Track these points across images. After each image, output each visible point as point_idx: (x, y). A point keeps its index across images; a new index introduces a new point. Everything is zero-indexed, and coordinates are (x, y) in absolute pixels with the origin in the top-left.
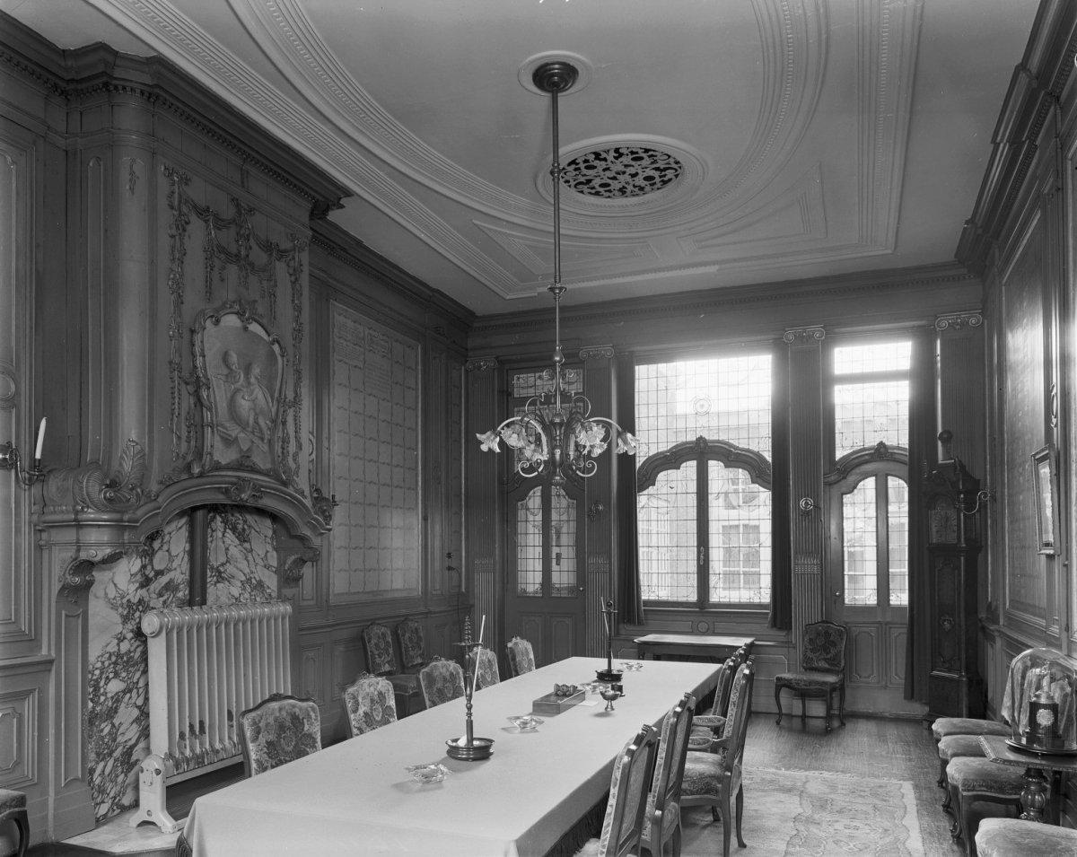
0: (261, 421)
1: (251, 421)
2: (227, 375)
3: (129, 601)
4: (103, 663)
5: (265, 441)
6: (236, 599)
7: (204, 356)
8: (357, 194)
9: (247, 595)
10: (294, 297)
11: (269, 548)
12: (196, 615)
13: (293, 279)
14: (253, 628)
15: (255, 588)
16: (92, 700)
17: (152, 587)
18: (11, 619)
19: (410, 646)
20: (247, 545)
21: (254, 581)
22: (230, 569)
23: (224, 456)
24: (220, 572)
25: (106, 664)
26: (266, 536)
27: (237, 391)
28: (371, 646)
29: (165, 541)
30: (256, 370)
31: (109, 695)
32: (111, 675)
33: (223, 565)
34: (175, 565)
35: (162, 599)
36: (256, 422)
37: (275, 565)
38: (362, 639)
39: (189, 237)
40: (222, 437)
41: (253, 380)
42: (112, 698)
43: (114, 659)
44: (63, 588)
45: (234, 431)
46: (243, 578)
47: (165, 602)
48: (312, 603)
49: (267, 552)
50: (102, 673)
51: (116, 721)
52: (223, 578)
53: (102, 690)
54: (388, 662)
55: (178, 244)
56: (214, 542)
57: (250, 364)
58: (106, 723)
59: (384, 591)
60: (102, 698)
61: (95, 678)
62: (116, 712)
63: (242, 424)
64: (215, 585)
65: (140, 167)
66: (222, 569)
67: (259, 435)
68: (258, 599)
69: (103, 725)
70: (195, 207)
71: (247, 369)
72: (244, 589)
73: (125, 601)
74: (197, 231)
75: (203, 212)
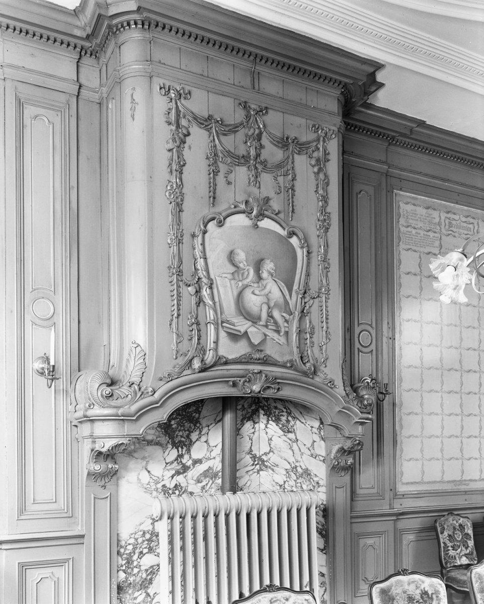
0: (276, 314)
1: (264, 315)
2: (233, 274)
3: (164, 486)
4: (136, 539)
5: (281, 334)
6: (281, 486)
7: (205, 259)
8: (391, 64)
9: (292, 483)
10: (317, 188)
11: (316, 438)
12: (231, 501)
13: (316, 169)
14: (182, 523)
15: (301, 476)
16: (124, 571)
17: (190, 474)
18: (52, 500)
19: (450, 544)
20: (291, 436)
21: (299, 469)
22: (273, 458)
23: (231, 350)
24: (263, 461)
25: (140, 540)
26: (312, 427)
27: (245, 287)
28: (444, 537)
29: (202, 433)
30: (268, 266)
31: (143, 568)
32: (145, 551)
33: (266, 454)
34: (213, 454)
35: (200, 485)
36: (270, 316)
37: (324, 454)
38: (435, 529)
39: (190, 148)
40: (229, 334)
41: (265, 275)
42: (146, 570)
43: (148, 536)
44: (89, 474)
45: (242, 325)
46: (288, 467)
47: (203, 488)
48: (375, 491)
49: (314, 441)
50: (135, 549)
51: (151, 591)
52: (266, 467)
53: (135, 563)
54: (466, 555)
55: (175, 157)
56: (256, 434)
57: (262, 260)
58: (140, 592)
59: (471, 480)
60: (136, 571)
61: (127, 552)
62: (151, 583)
63: (254, 319)
64: (258, 472)
65: (139, 96)
66: (264, 458)
67: (274, 328)
68: (305, 487)
69: (136, 594)
70: (195, 118)
71: (258, 266)
72: (289, 477)
73: (159, 486)
74: (199, 139)
75: (206, 122)
